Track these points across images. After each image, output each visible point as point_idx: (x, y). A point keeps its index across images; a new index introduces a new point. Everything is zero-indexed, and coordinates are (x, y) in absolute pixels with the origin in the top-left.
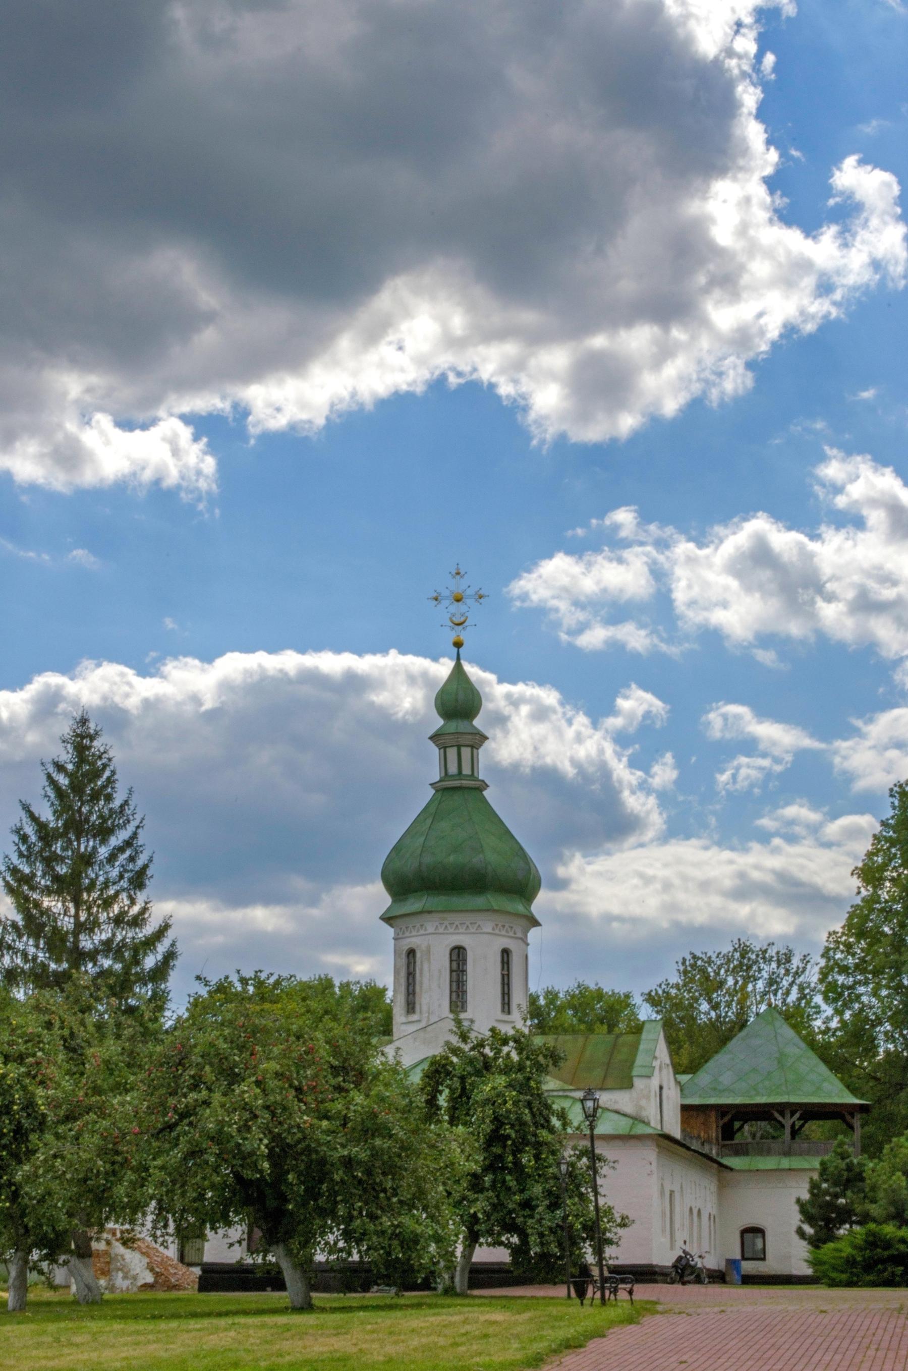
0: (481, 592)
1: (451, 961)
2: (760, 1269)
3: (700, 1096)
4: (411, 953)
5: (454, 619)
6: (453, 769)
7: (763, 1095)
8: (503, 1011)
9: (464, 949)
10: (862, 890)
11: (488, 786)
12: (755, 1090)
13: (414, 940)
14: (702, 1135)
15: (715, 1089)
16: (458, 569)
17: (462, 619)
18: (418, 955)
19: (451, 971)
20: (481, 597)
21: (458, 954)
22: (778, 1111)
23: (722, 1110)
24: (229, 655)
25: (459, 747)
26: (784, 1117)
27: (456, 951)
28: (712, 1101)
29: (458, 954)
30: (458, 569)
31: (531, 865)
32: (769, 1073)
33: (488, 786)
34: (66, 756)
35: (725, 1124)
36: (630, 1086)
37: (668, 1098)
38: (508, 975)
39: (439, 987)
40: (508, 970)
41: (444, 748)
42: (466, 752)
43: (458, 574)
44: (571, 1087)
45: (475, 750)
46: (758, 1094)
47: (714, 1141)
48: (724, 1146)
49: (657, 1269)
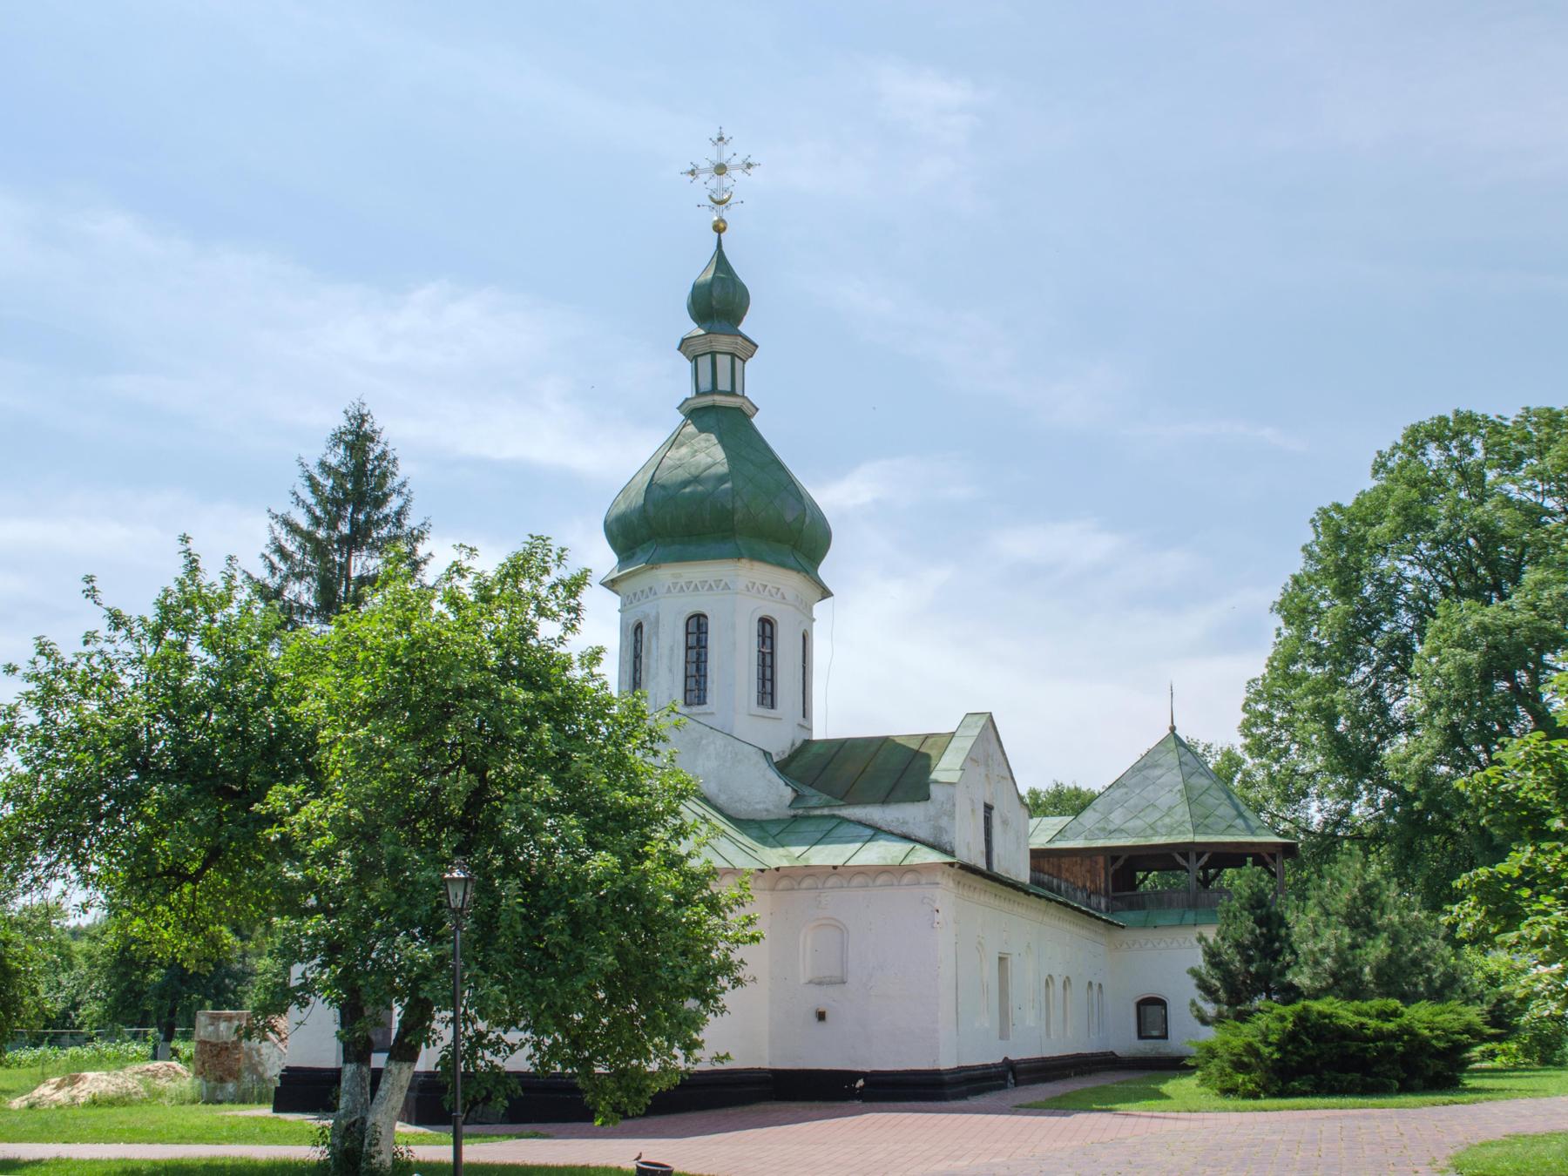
0: (750, 160)
1: (687, 633)
2: (1161, 1050)
3: (1086, 839)
4: (639, 628)
5: (714, 196)
6: (706, 384)
7: (1162, 835)
8: (761, 702)
9: (705, 617)
10: (1283, 631)
11: (757, 409)
12: (1152, 829)
13: (645, 609)
14: (1088, 884)
15: (1104, 829)
16: (721, 133)
17: (726, 197)
18: (645, 629)
19: (688, 648)
20: (749, 166)
21: (697, 626)
22: (1180, 854)
23: (1112, 854)
24: (819, 572)
25: (713, 354)
26: (1188, 861)
27: (693, 622)
28: (1100, 843)
29: (697, 626)
30: (721, 133)
31: (807, 501)
32: (1170, 808)
33: (757, 409)
34: (336, 458)
35: (1116, 871)
36: (927, 797)
37: (1005, 822)
38: (772, 654)
39: (670, 670)
40: (772, 648)
41: (694, 359)
42: (723, 362)
43: (721, 139)
44: (842, 803)
45: (738, 362)
46: (1156, 833)
47: (1103, 892)
48: (1115, 898)
49: (947, 1078)
